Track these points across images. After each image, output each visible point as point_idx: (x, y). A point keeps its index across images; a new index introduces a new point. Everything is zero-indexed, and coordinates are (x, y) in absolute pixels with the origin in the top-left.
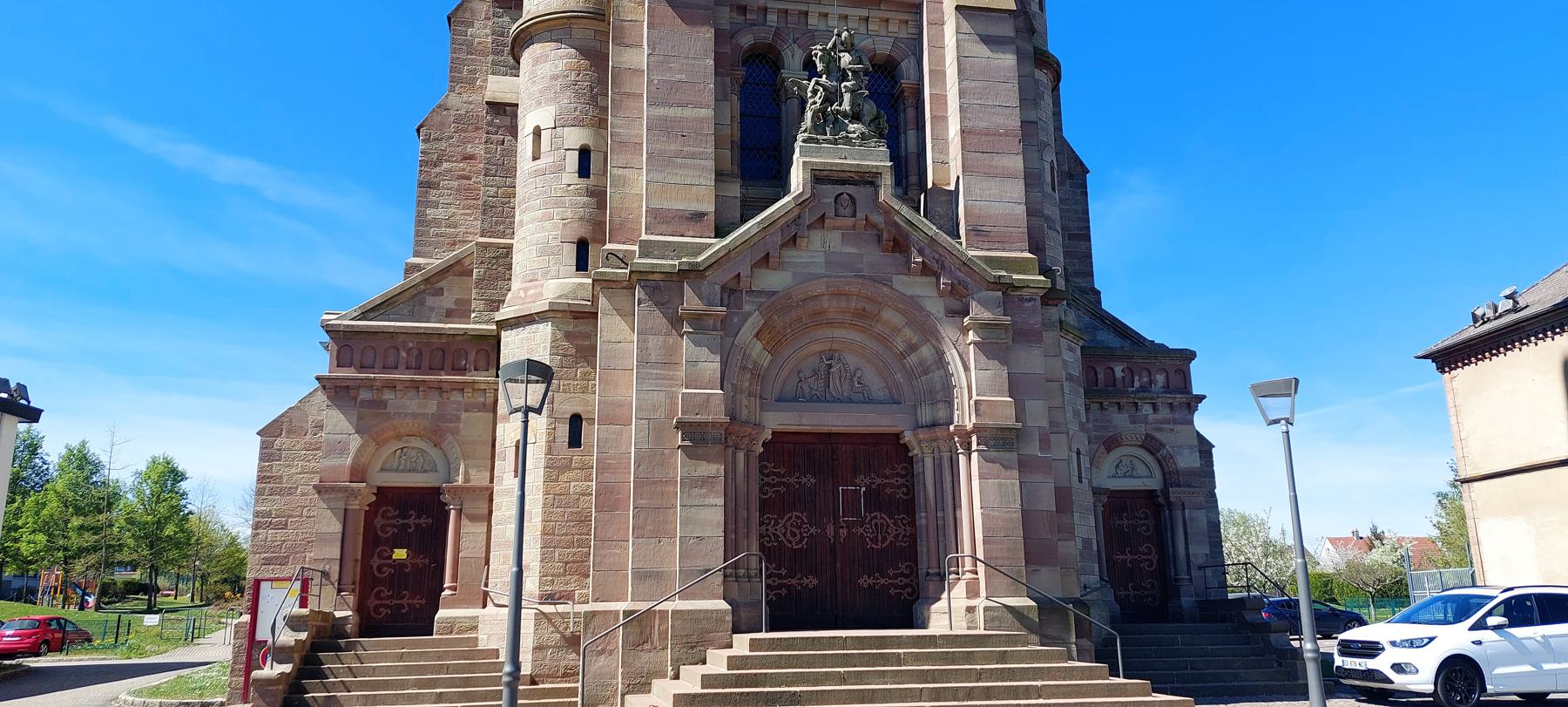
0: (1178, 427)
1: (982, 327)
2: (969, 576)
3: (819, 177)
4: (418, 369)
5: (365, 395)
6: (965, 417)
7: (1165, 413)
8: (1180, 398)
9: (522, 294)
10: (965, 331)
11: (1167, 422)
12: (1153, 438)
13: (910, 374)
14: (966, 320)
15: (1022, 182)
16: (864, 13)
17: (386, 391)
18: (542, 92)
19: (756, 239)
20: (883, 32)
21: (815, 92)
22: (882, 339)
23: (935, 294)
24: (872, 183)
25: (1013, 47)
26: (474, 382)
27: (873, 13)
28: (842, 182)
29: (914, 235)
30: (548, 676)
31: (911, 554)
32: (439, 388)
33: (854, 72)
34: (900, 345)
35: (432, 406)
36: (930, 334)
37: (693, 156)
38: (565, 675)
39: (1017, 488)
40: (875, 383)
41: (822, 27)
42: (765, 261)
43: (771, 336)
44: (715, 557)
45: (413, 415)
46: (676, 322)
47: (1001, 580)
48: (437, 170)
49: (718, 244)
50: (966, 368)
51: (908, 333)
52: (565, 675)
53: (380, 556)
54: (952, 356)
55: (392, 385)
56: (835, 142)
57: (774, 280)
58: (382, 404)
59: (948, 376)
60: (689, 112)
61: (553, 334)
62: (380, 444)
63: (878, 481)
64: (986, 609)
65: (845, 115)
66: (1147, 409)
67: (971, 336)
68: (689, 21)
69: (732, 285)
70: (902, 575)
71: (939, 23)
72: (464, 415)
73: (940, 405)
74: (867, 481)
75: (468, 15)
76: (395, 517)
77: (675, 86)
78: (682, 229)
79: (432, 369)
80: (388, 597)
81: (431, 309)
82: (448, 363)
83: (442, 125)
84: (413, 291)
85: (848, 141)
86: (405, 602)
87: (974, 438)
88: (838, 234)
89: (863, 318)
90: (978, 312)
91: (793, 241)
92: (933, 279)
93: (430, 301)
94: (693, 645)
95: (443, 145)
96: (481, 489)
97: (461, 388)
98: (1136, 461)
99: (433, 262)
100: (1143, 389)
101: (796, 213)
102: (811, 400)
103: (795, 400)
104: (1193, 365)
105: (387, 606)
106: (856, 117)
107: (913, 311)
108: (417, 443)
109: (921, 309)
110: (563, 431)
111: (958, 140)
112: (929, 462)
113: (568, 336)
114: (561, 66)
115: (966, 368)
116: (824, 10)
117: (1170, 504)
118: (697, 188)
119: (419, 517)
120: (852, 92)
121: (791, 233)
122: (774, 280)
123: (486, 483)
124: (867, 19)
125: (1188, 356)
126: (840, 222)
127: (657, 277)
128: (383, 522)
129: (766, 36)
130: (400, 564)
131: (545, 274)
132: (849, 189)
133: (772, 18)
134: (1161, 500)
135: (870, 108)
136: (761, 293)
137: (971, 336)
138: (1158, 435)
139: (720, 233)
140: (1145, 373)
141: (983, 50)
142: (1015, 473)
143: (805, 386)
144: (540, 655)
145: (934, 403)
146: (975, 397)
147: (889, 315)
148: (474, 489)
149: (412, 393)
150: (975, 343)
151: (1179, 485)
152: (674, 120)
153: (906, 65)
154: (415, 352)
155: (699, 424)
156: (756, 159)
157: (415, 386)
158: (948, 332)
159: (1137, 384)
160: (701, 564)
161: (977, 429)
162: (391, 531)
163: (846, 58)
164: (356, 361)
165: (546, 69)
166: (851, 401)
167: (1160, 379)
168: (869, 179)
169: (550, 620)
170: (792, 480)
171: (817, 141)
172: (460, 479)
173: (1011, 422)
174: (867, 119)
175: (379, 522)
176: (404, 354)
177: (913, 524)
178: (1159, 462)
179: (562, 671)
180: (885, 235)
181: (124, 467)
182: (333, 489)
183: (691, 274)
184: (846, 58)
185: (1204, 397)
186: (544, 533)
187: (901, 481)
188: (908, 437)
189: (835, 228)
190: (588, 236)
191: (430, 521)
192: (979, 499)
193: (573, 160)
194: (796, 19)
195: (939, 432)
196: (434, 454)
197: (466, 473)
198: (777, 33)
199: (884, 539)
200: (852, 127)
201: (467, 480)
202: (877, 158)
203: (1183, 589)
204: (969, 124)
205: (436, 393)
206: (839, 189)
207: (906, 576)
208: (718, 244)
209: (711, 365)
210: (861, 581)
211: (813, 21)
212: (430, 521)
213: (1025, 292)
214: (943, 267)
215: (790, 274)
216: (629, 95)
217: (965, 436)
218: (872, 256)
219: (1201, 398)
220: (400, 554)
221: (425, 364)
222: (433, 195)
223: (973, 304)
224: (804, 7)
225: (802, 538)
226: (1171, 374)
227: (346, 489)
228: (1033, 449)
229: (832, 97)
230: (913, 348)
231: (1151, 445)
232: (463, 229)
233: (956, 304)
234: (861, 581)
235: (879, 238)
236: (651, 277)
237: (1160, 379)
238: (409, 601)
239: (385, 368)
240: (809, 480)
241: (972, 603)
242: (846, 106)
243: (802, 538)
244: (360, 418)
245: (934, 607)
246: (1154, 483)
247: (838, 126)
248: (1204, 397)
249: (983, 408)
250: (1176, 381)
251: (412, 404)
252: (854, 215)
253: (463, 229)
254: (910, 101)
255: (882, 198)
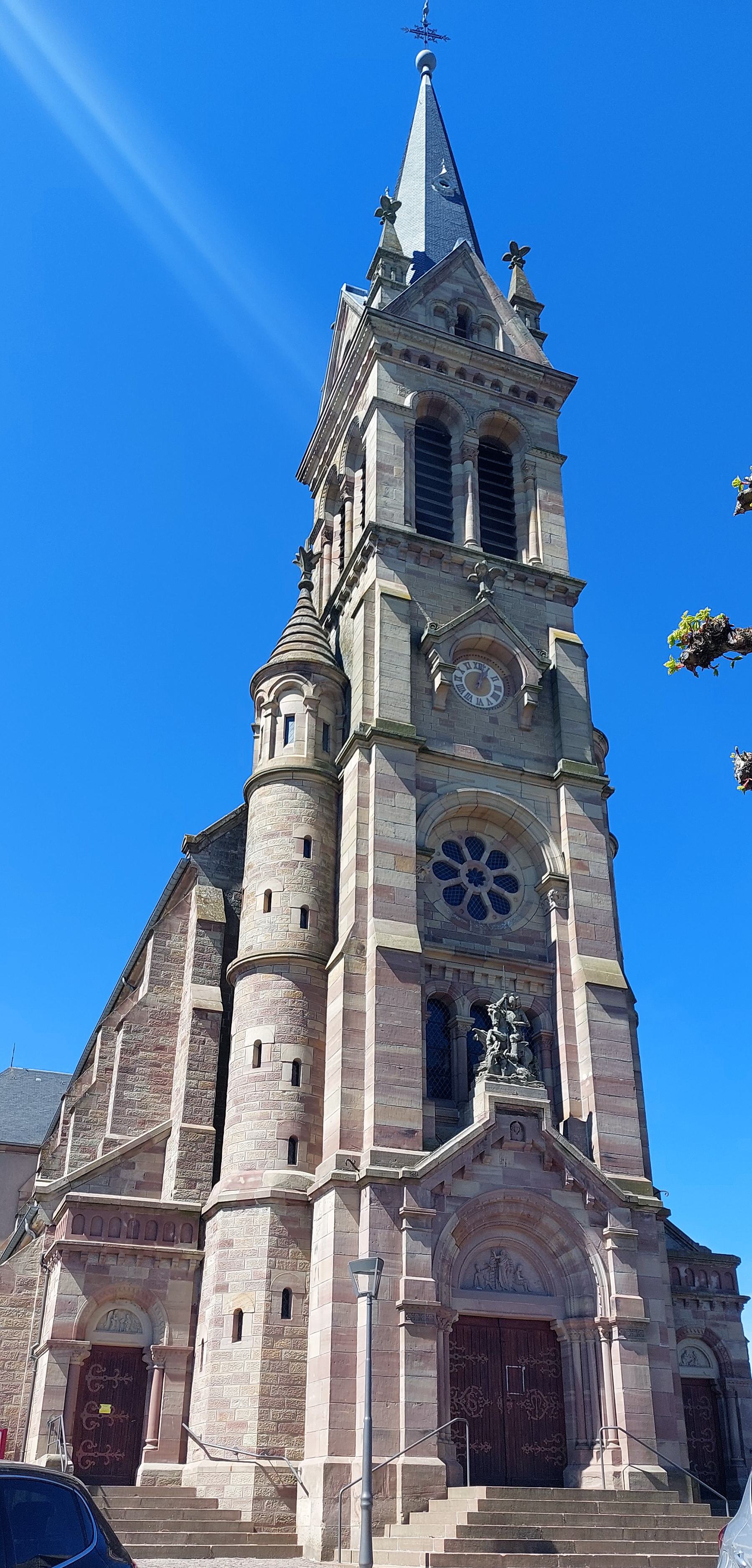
0: (730, 1324)
1: (617, 1237)
2: (612, 1445)
3: (500, 1109)
4: (135, 1239)
5: (92, 1260)
6: (606, 1310)
7: (719, 1311)
8: (731, 1298)
9: (242, 1180)
10: (604, 1238)
11: (721, 1318)
12: (711, 1332)
13: (560, 1271)
14: (606, 1231)
15: (637, 1120)
16: (514, 976)
17: (109, 1257)
18: (264, 1013)
19: (457, 1154)
20: (526, 991)
21: (492, 1042)
22: (540, 1241)
23: (581, 1206)
24: (536, 1116)
25: (626, 1016)
26: (182, 1253)
27: (520, 977)
28: (516, 1113)
29: (568, 1159)
30: (265, 1525)
31: (560, 1426)
32: (153, 1257)
33: (517, 1026)
34: (554, 1247)
35: (145, 1273)
36: (578, 1240)
37: (407, 1084)
38: (278, 1525)
39: (648, 1373)
40: (532, 1279)
41: (483, 984)
42: (461, 1172)
43: (462, 1234)
44: (431, 1422)
45: (130, 1280)
46: (397, 1219)
47: (640, 1449)
48: (134, 1057)
49: (431, 1157)
50: (607, 1271)
51: (561, 1237)
52: (278, 1525)
53: (89, 1410)
54: (595, 1259)
55: (115, 1253)
56: (509, 1081)
57: (467, 1188)
58: (104, 1269)
59: (592, 1275)
60: (403, 1050)
61: (272, 1217)
62: (99, 1305)
63: (535, 1361)
64: (631, 1474)
65: (513, 1059)
66: (705, 1306)
67: (609, 1244)
68: (403, 980)
69: (437, 1191)
70: (554, 1444)
71: (568, 990)
72: (170, 1282)
73: (587, 1300)
74: (526, 1361)
75: (167, 929)
76: (102, 1374)
77: (394, 1030)
78: (400, 1142)
79: (147, 1240)
80: (94, 1450)
81: (125, 1181)
82: (160, 1235)
83: (141, 1019)
84: (111, 1165)
86: (107, 1455)
87: (615, 1329)
89: (527, 1223)
90: (613, 1224)
91: (481, 1157)
92: (580, 1195)
93: (124, 1173)
94: (419, 1497)
95: (140, 1036)
96: (182, 1351)
97: (170, 1257)
98: (697, 1352)
99: (132, 1139)
100: (702, 1288)
101: (483, 1136)
102: (484, 1290)
103: (473, 1288)
104: (739, 1270)
105: (92, 1458)
106: (520, 1062)
107: (565, 1218)
108: (128, 1306)
109: (572, 1219)
110: (278, 1301)
111: (590, 1084)
112: (576, 1347)
113: (283, 1220)
114: (281, 993)
115: (607, 1271)
116: (486, 971)
117: (725, 1391)
118: (412, 1111)
119: (122, 1375)
121: (479, 1149)
122: (467, 1188)
123: (185, 1345)
124: (515, 981)
125: (734, 1261)
126: (514, 1144)
127: (384, 1181)
128: (94, 1378)
129: (445, 988)
130: (105, 1419)
131: (262, 1166)
132: (520, 1119)
133: (449, 975)
134: (718, 1388)
135: (528, 1055)
136: (458, 1198)
137: (609, 1244)
138: (714, 1330)
139: (429, 1145)
140: (703, 1275)
141: (605, 1016)
142: (645, 1359)
143: (481, 1277)
144: (259, 1505)
145: (581, 1297)
146: (614, 1295)
147: (547, 1221)
148: (175, 1351)
149: (130, 1260)
150: (614, 1250)
151: (732, 1376)
152: (395, 1055)
153: (543, 1018)
154: (133, 1223)
155: (419, 1306)
156: (446, 1089)
157: (134, 1253)
158: (591, 1236)
159: (697, 1284)
160: (422, 1426)
161: (618, 1322)
162: (100, 1386)
163: (511, 1016)
164: (87, 1228)
165: (267, 995)
166: (515, 1291)
167: (714, 1279)
168: (534, 1113)
169: (266, 1473)
170: (471, 1358)
171: (496, 1080)
172: (165, 1340)
173: (641, 1317)
174: (527, 1063)
175: (90, 1378)
176: (126, 1225)
177: (561, 1399)
178: (715, 1353)
179: (275, 1521)
180: (546, 1157)
182: (63, 1345)
183: (411, 1180)
184: (511, 1016)
185: (748, 1298)
186: (262, 1394)
187: (552, 1362)
188: (560, 1325)
189: (510, 1149)
190: (297, 1135)
191: (131, 1379)
192: (619, 1382)
193: (288, 1069)
195: (587, 1322)
196: (141, 1316)
197: (170, 1335)
199: (540, 1413)
201: (170, 1342)
202: (539, 1097)
203: (739, 1470)
204: (599, 1073)
205: (148, 1261)
206: (514, 1118)
207: (558, 1445)
208: (431, 1157)
209: (425, 1257)
210: (524, 1448)
211: (477, 979)
212: (131, 1379)
213: (645, 1210)
214: (588, 1186)
215: (478, 1185)
216: (354, 1031)
217: (608, 1326)
218: (536, 1173)
219: (746, 1299)
220: (105, 1409)
221: (142, 1235)
222: (130, 1079)
223: (610, 1218)
224: (471, 969)
225: (479, 1409)
226: (722, 1274)
227: (73, 1346)
228: (656, 1340)
229: (505, 1044)
230: (564, 1249)
231: (710, 1339)
232: (152, 1110)
233: (597, 1217)
234: (524, 1448)
235: (541, 1158)
236: (380, 1181)
237: (714, 1279)
238: (113, 1454)
239: (110, 1237)
240: (483, 1358)
241: (618, 1469)
242: (513, 1053)
243: (479, 1409)
244: (87, 1281)
245: (586, 1472)
246: (711, 1373)
247: (510, 1071)
248: (748, 1298)
249: (621, 1304)
250: (726, 1281)
251: (130, 1270)
252: (523, 1140)
253: (152, 1110)
254: (546, 1046)
255: (544, 1128)
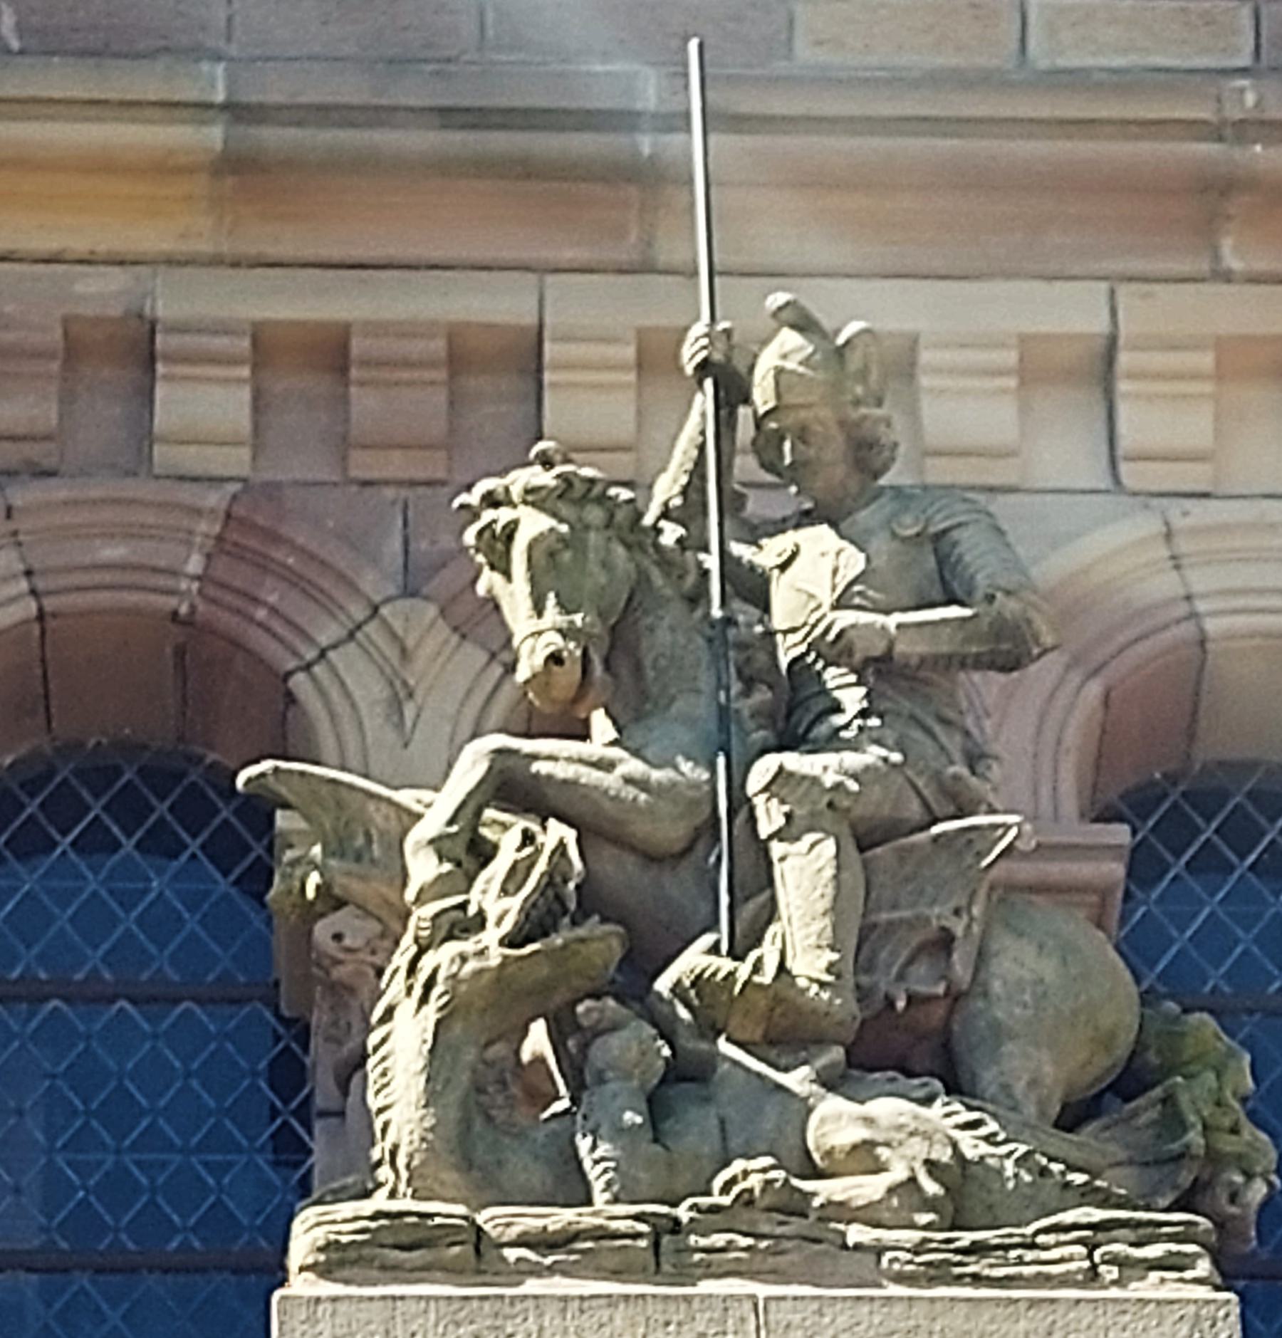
27: (1142, 313)
33: (879, 669)
65: (785, 1027)
85: (795, 1232)
88: (1003, 942)
106: (905, 1043)
120: (866, 837)
133: (203, 411)
174: (1038, 1067)
181: (883, 1158)
194: (427, 405)
198: (249, 531)
200: (835, 1122)
224: (501, 304)
242: (803, 941)
